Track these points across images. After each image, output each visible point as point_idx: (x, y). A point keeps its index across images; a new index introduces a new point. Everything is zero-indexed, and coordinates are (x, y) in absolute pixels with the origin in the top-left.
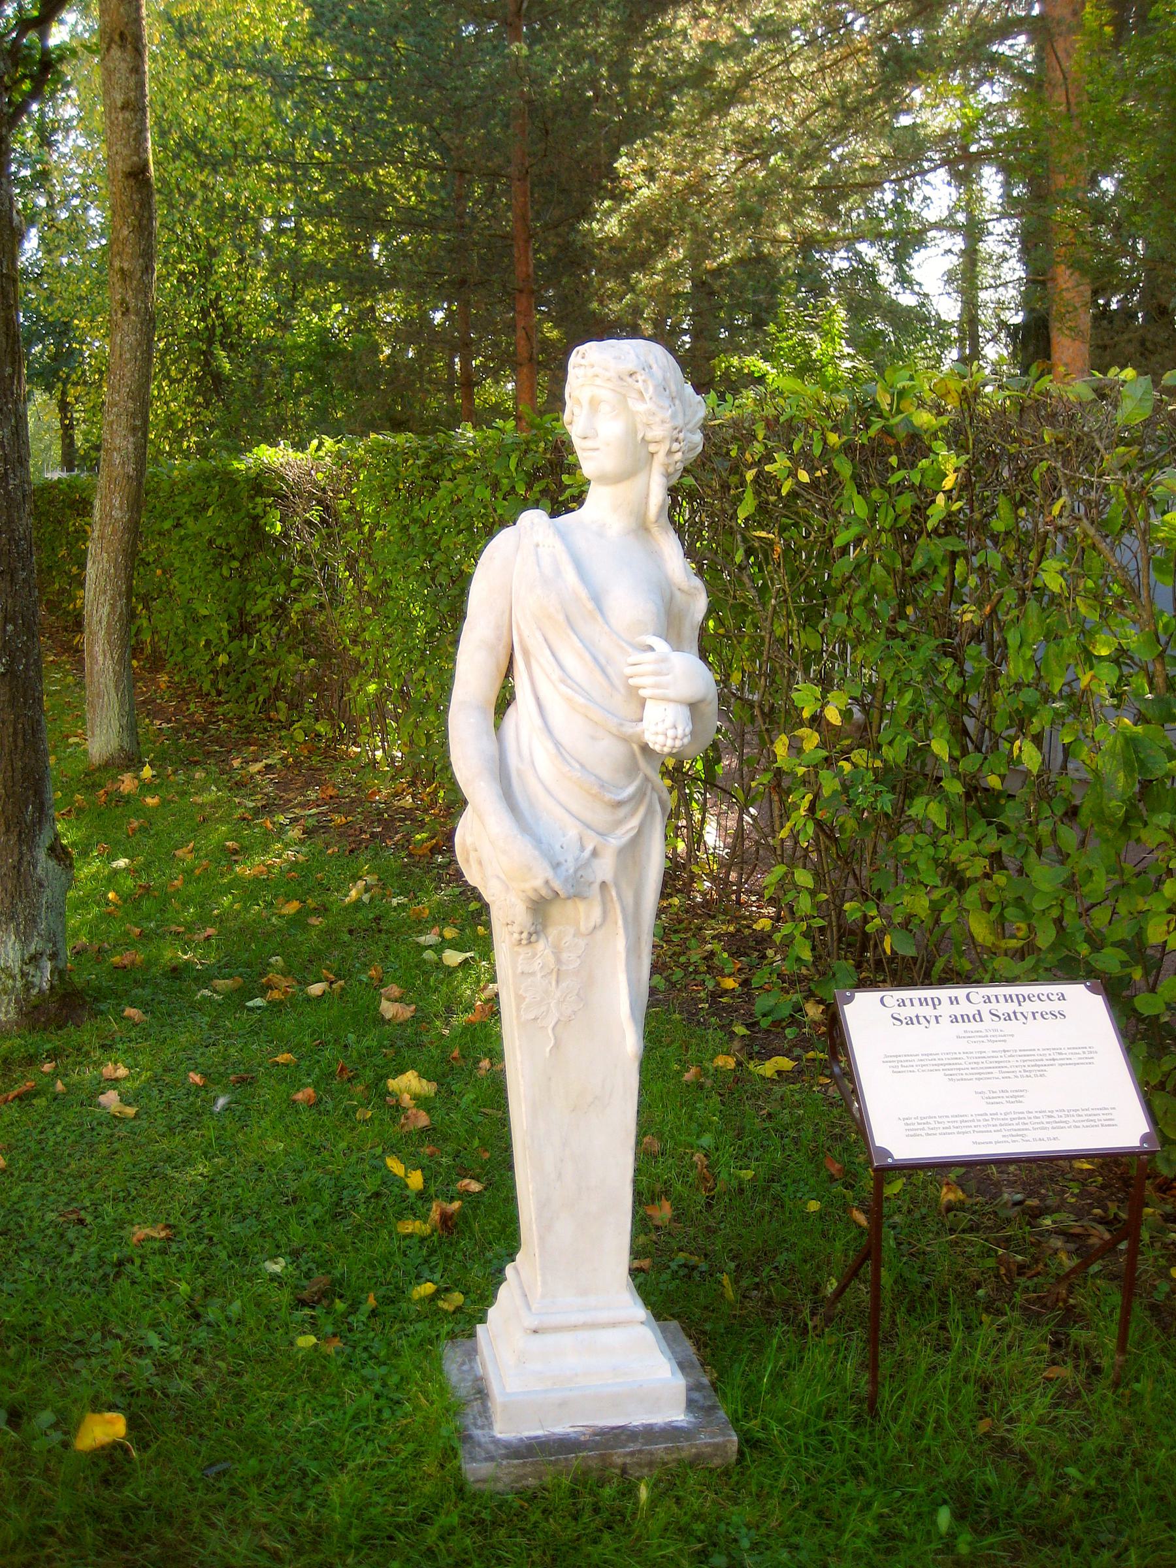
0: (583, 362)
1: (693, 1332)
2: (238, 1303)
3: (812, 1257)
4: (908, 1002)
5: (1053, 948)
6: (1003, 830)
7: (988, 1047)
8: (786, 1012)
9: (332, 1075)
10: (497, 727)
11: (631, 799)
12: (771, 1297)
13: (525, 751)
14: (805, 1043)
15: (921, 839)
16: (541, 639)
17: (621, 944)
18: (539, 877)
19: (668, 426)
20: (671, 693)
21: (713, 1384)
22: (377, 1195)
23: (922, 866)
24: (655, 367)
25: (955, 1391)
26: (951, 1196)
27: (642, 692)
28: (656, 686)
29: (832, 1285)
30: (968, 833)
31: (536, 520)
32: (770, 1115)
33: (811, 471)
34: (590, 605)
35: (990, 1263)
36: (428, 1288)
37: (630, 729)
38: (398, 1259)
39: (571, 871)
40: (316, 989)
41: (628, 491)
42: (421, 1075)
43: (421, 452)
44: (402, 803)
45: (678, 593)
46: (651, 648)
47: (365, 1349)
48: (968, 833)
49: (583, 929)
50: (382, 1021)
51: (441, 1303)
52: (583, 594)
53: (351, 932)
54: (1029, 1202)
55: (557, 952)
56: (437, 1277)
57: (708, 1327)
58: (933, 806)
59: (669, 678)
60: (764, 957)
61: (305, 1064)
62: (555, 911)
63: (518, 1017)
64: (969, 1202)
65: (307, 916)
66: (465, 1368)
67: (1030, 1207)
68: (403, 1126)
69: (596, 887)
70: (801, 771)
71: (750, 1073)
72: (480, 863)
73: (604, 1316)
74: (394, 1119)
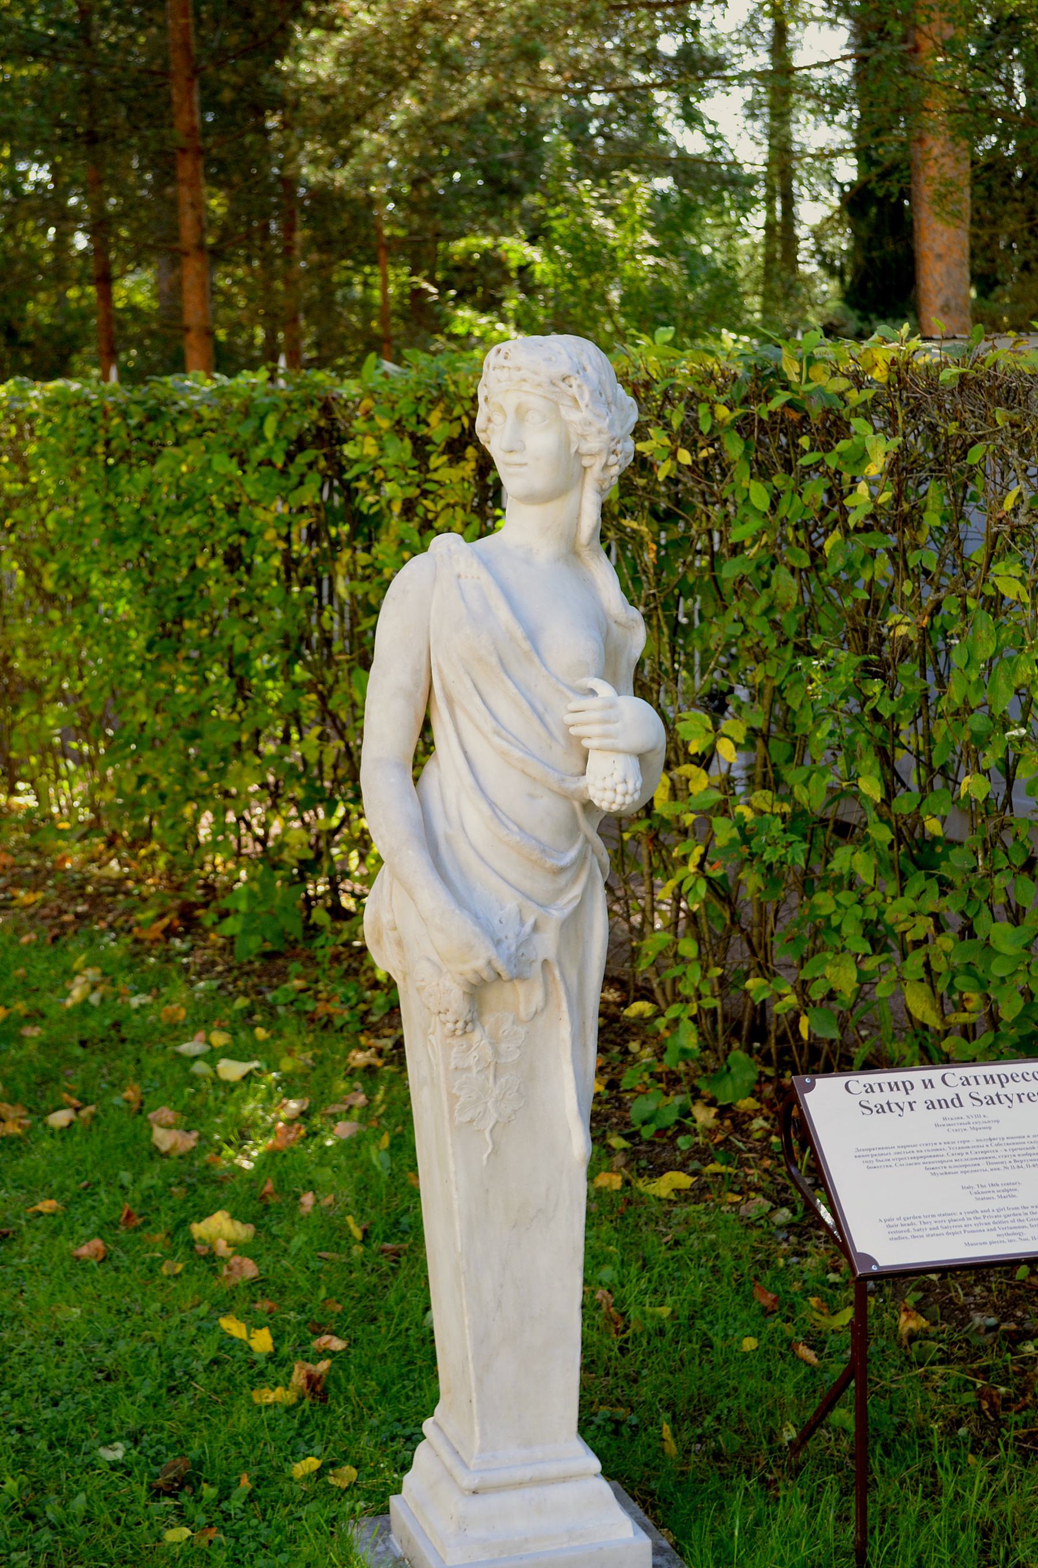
0: (506, 363)
1: (636, 1493)
2: (82, 1497)
3: (759, 1401)
4: (876, 1088)
5: (1017, 1022)
6: (945, 886)
7: (971, 1136)
8: (671, 1117)
9: (114, 1225)
10: (416, 779)
11: (573, 863)
12: (720, 1448)
13: (453, 813)
14: (702, 1154)
15: (846, 897)
16: (469, 685)
17: (565, 1031)
18: (481, 957)
19: (605, 437)
20: (621, 744)
21: (675, 1546)
22: (215, 1362)
23: (846, 930)
24: (589, 368)
25: (953, 1539)
26: (912, 1324)
27: (585, 743)
28: (605, 736)
29: (789, 1434)
30: (902, 890)
31: (453, 547)
32: (677, 1243)
33: (693, 448)
34: (526, 646)
35: (969, 1397)
36: (312, 1463)
37: (573, 785)
38: (267, 1435)
39: (513, 948)
40: (60, 1118)
41: (558, 511)
42: (234, 1216)
43: (133, 408)
44: (105, 872)
45: (614, 626)
46: (592, 692)
47: (253, 1537)
48: (902, 890)
49: (523, 1014)
50: (155, 1153)
51: (332, 1480)
52: (519, 633)
53: (83, 1044)
54: (1004, 1327)
55: (494, 1044)
56: (318, 1449)
57: (653, 1485)
58: (860, 856)
59: (618, 725)
60: (626, 1052)
61: (78, 1212)
62: (492, 996)
63: (452, 1120)
64: (933, 1330)
65: (20, 1025)
66: (379, 1549)
67: (1007, 1332)
68: (228, 1277)
69: (538, 965)
70: (689, 819)
71: (641, 1195)
72: (399, 943)
73: (553, 1469)
74: (214, 1271)
